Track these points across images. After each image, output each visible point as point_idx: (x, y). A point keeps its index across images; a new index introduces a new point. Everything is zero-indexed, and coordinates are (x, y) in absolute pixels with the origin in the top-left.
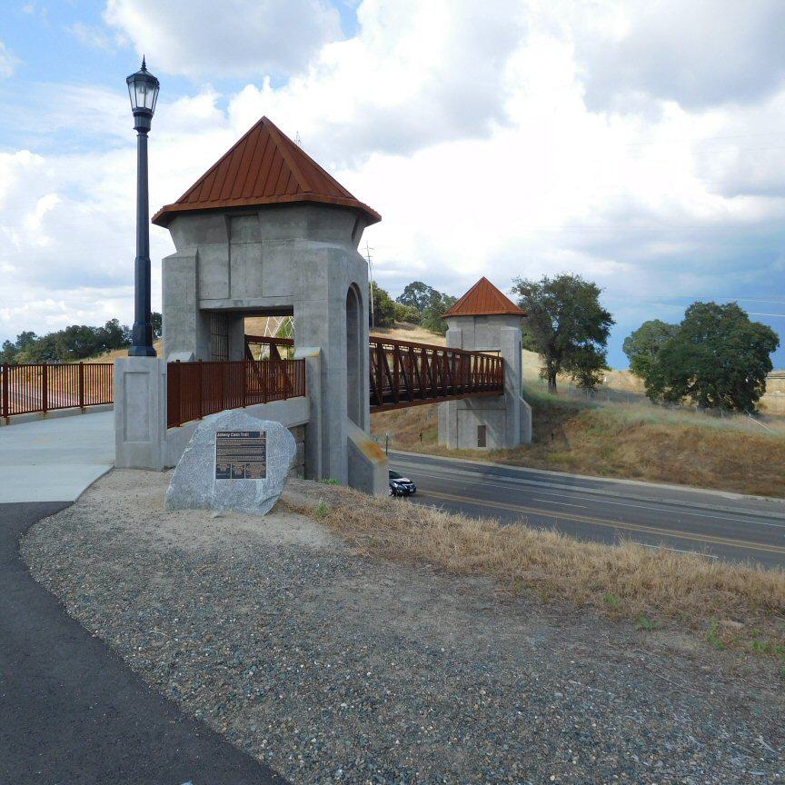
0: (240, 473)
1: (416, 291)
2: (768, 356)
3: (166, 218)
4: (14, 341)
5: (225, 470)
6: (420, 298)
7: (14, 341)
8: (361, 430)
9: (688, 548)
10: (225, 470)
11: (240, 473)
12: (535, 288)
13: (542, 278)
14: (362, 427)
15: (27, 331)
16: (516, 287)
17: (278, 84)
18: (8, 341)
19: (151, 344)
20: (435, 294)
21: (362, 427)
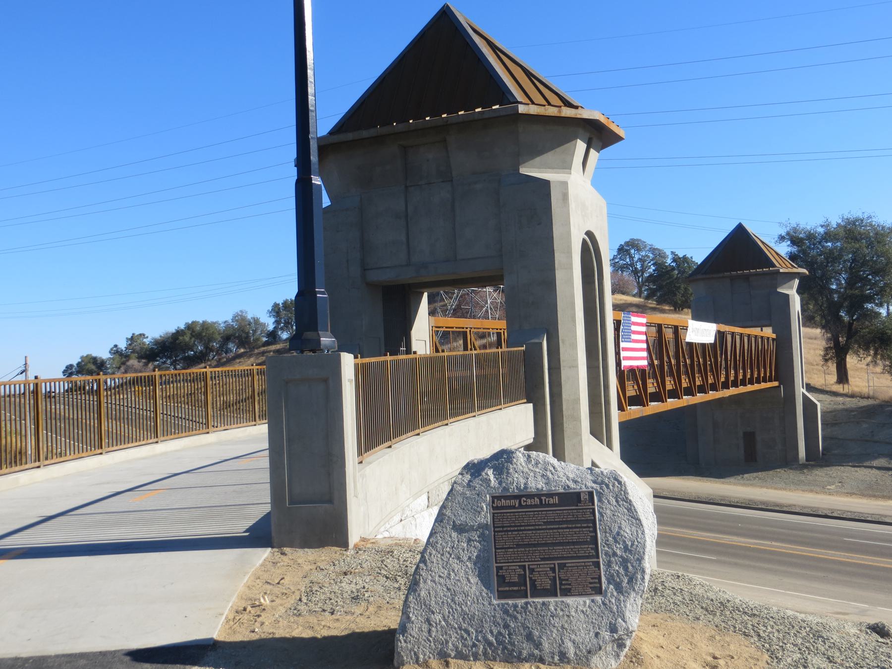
0: (547, 583)
1: (632, 251)
2: (512, 398)
3: (327, 147)
4: (123, 345)
5: (516, 579)
6: (640, 260)
7: (123, 345)
8: (606, 448)
9: (501, 506)
10: (516, 579)
11: (547, 583)
12: (811, 236)
13: (821, 221)
14: (609, 445)
15: (137, 333)
16: (784, 234)
17: (256, 321)
18: (116, 346)
19: (273, 331)
20: (659, 254)
21: (609, 445)
